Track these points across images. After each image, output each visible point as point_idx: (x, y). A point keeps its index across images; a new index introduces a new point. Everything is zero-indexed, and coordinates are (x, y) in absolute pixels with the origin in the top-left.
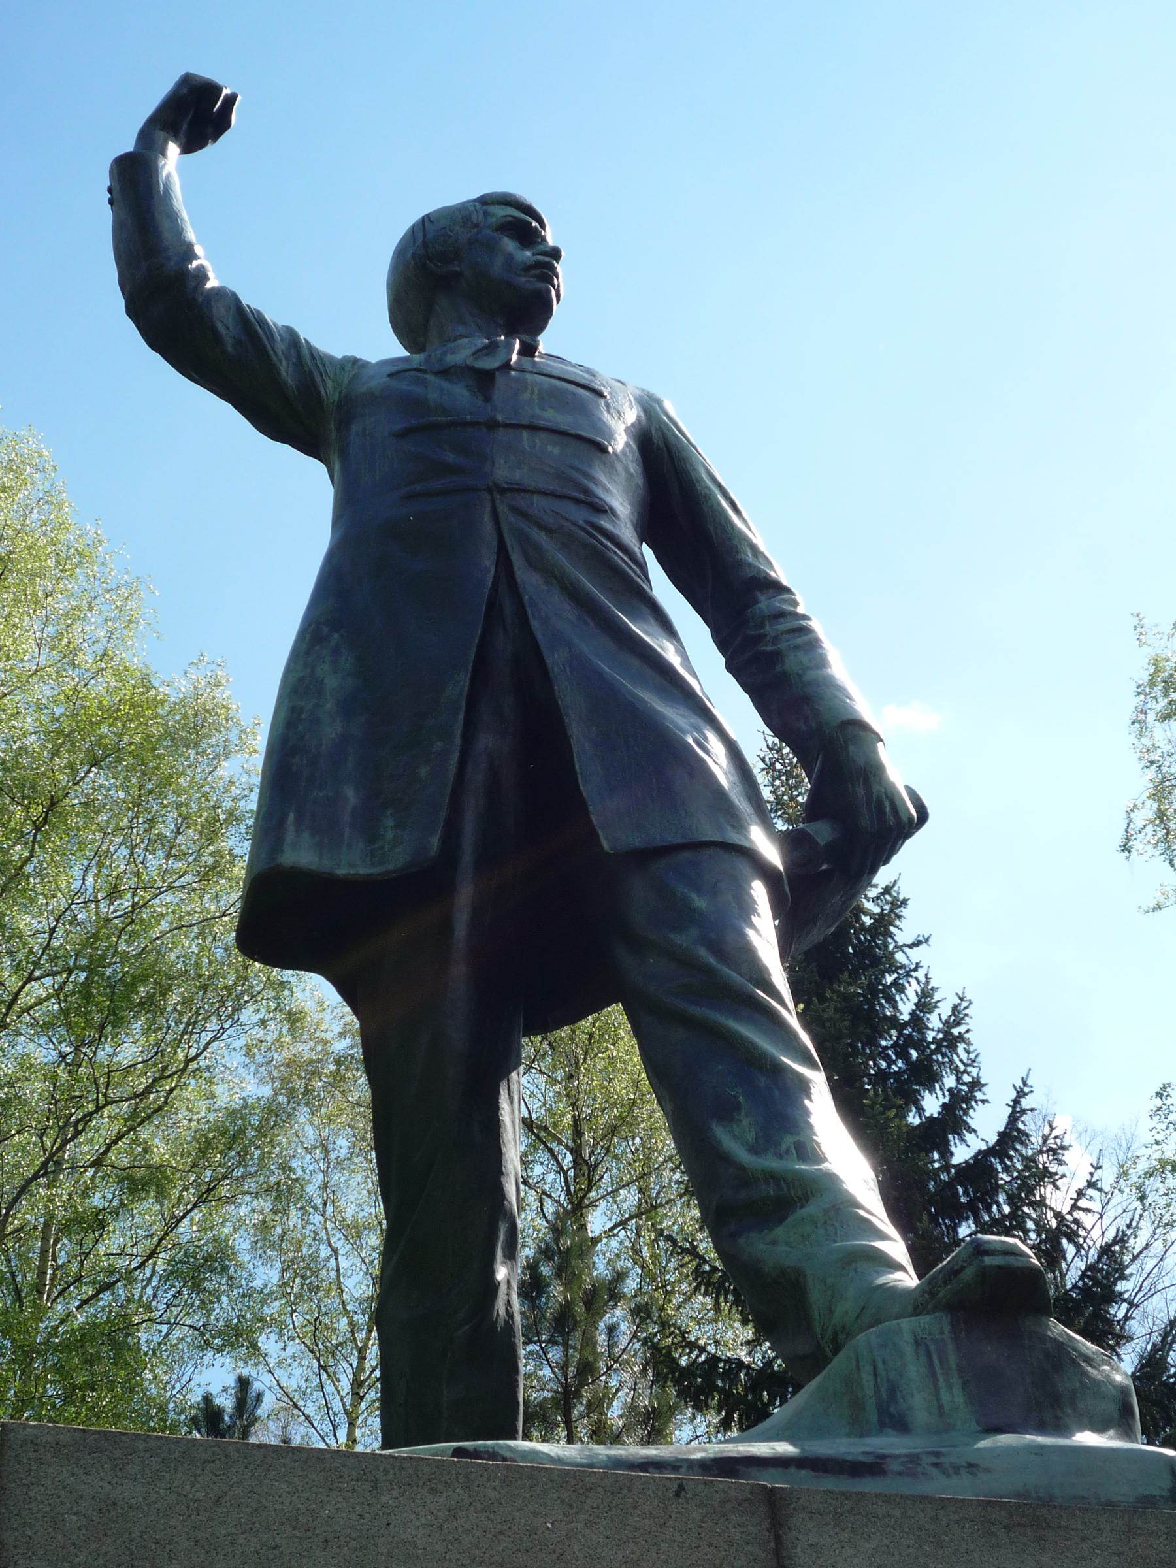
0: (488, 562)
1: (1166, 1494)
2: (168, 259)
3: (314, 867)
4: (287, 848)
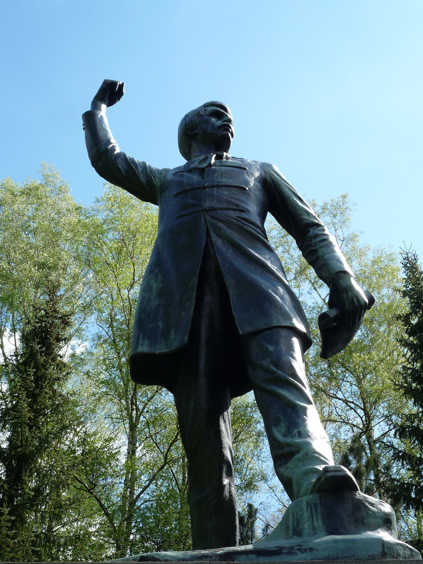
0: (204, 237)
1: (379, 554)
2: (101, 146)
3: (148, 352)
4: (139, 346)
